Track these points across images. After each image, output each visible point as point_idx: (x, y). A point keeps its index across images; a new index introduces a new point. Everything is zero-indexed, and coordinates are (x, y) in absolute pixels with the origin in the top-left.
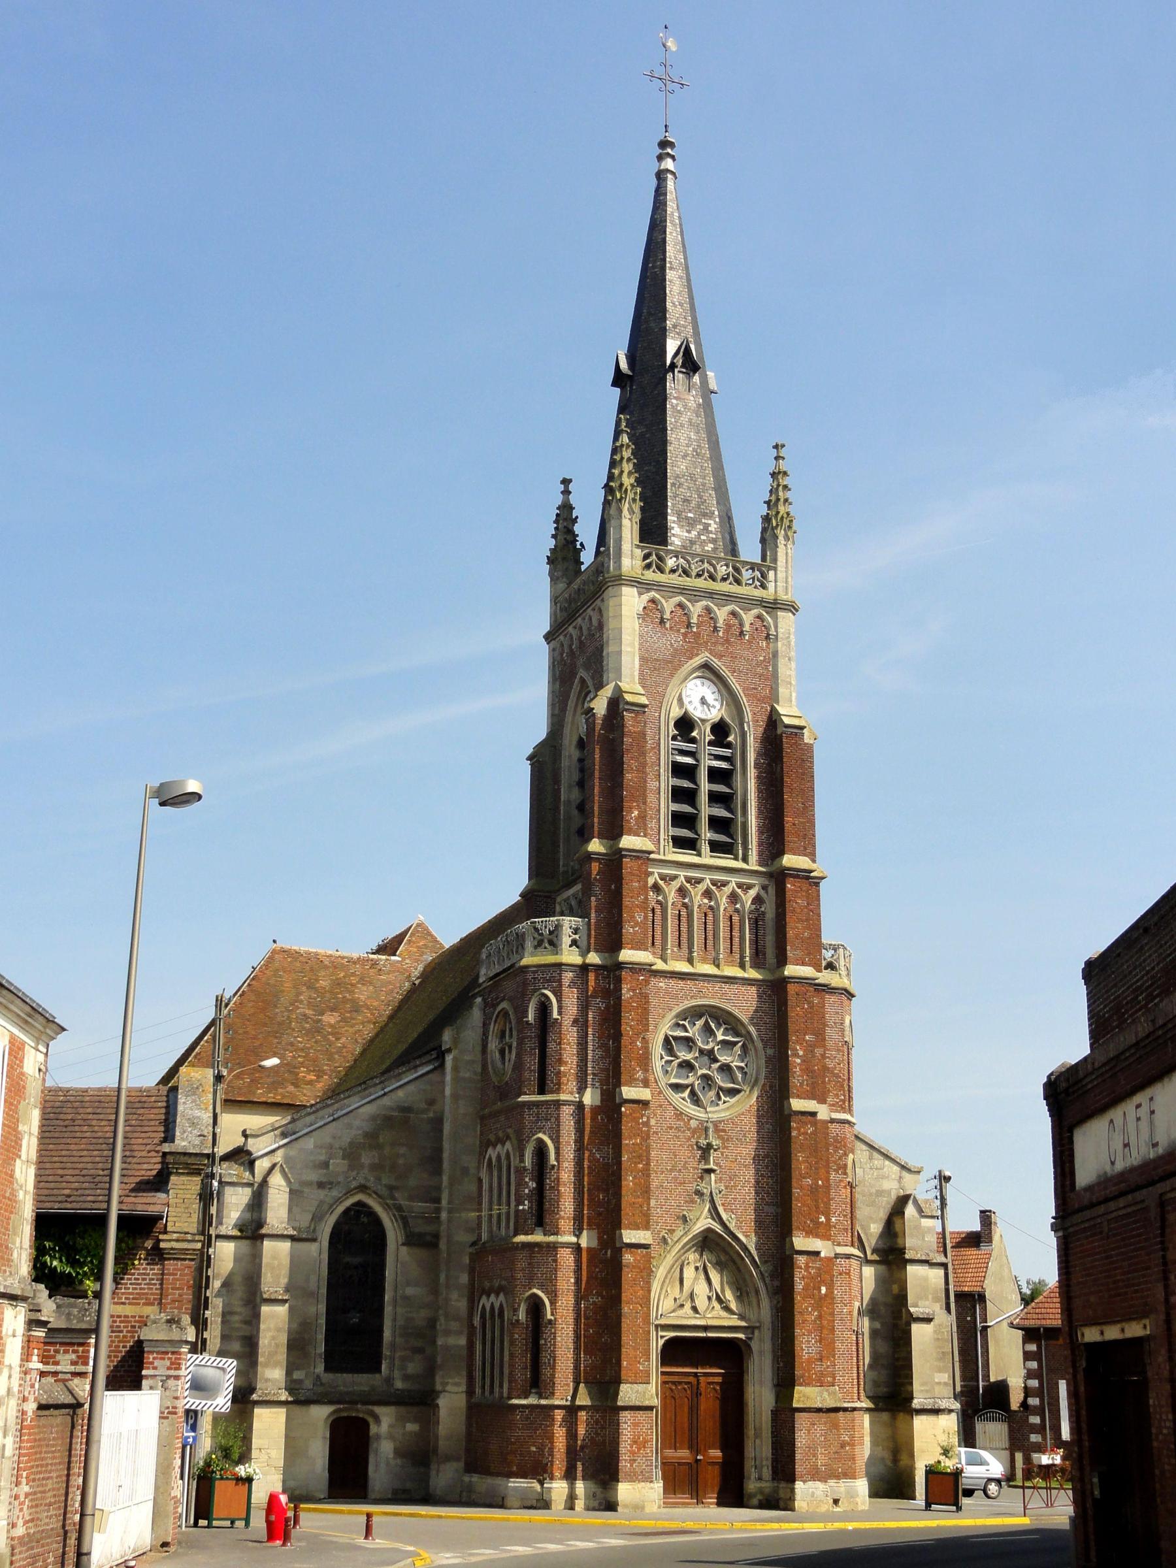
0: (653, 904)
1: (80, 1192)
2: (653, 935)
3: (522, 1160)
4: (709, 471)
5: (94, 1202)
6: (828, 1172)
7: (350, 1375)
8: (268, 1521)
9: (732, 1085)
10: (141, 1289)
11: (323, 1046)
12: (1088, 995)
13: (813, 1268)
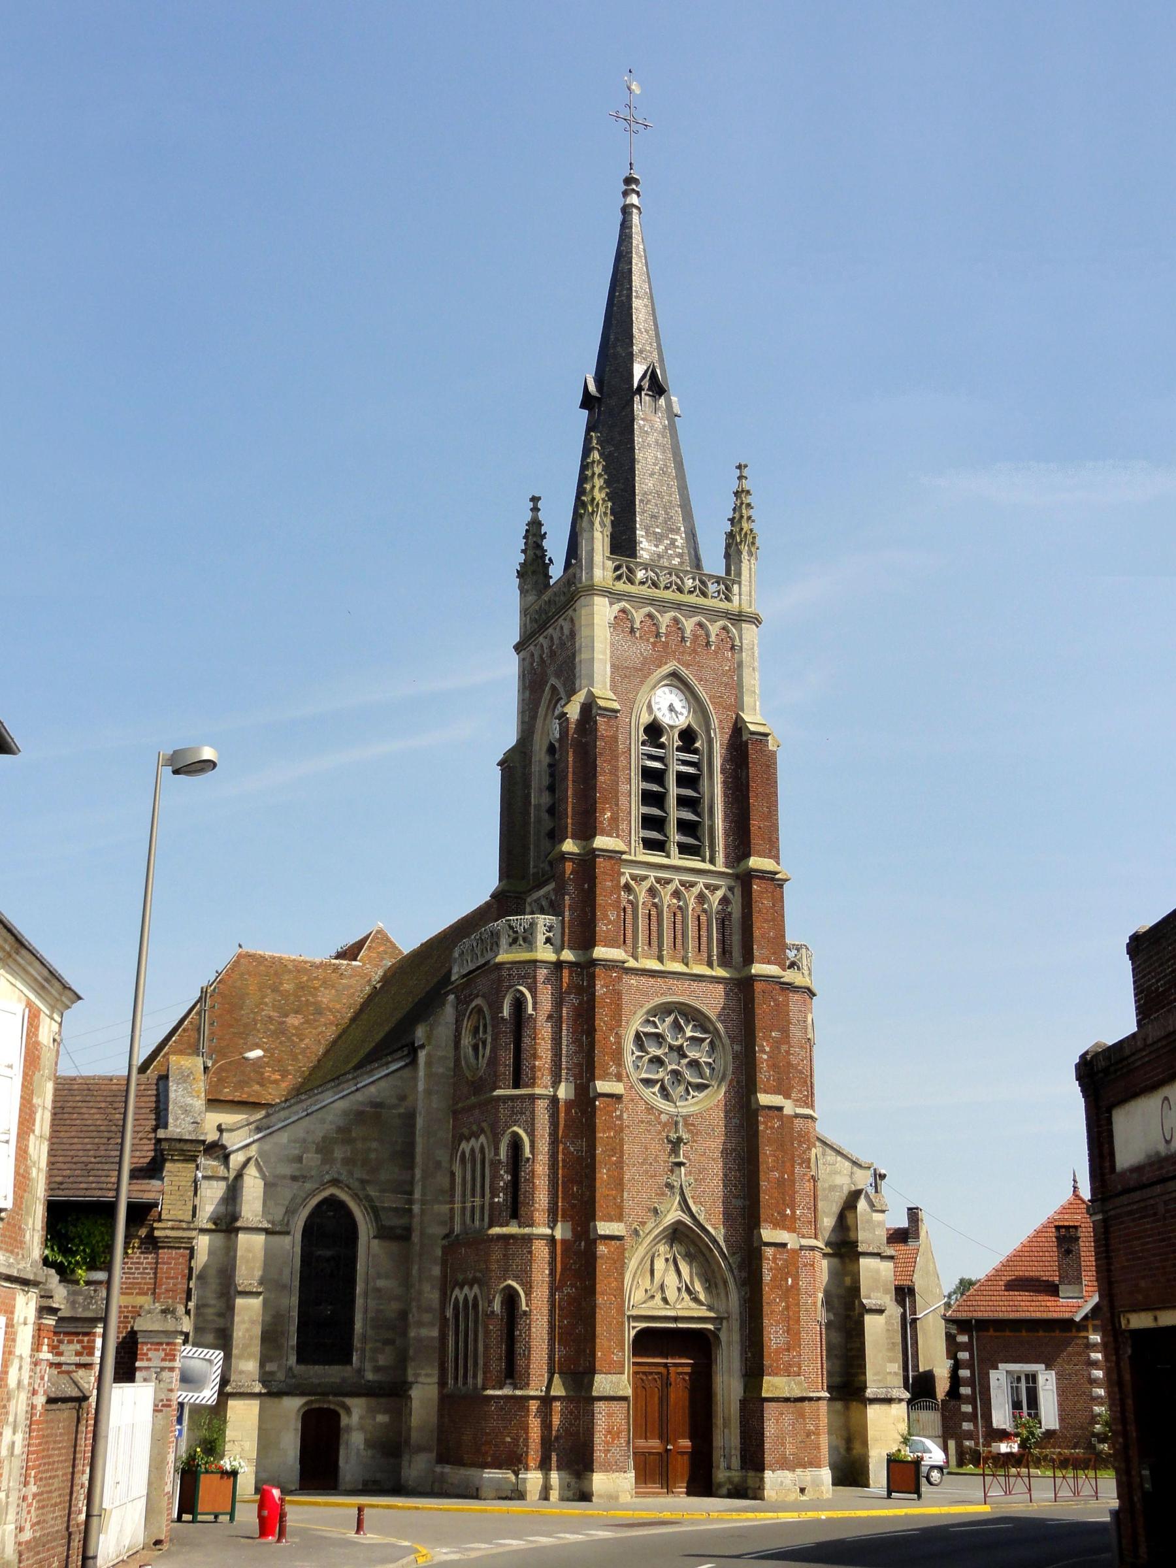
0: (624, 903)
1: (71, 1179)
2: (624, 934)
3: (497, 1153)
4: (675, 489)
5: (86, 1189)
6: (793, 1166)
7: (322, 1367)
8: (260, 1516)
9: (700, 1080)
10: (134, 1278)
11: (287, 1046)
12: (1133, 970)
13: (780, 1259)
